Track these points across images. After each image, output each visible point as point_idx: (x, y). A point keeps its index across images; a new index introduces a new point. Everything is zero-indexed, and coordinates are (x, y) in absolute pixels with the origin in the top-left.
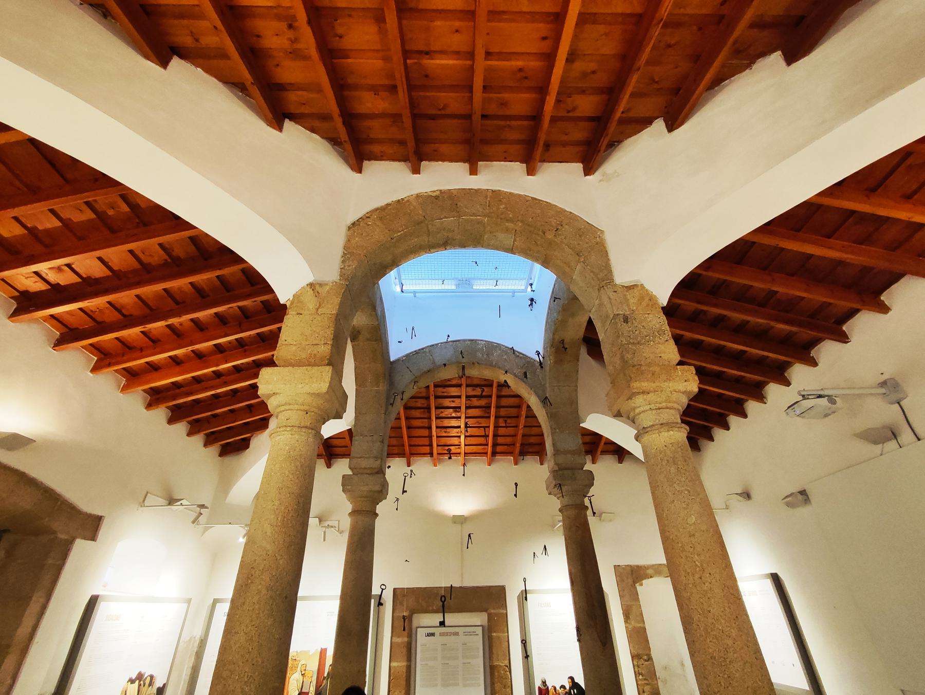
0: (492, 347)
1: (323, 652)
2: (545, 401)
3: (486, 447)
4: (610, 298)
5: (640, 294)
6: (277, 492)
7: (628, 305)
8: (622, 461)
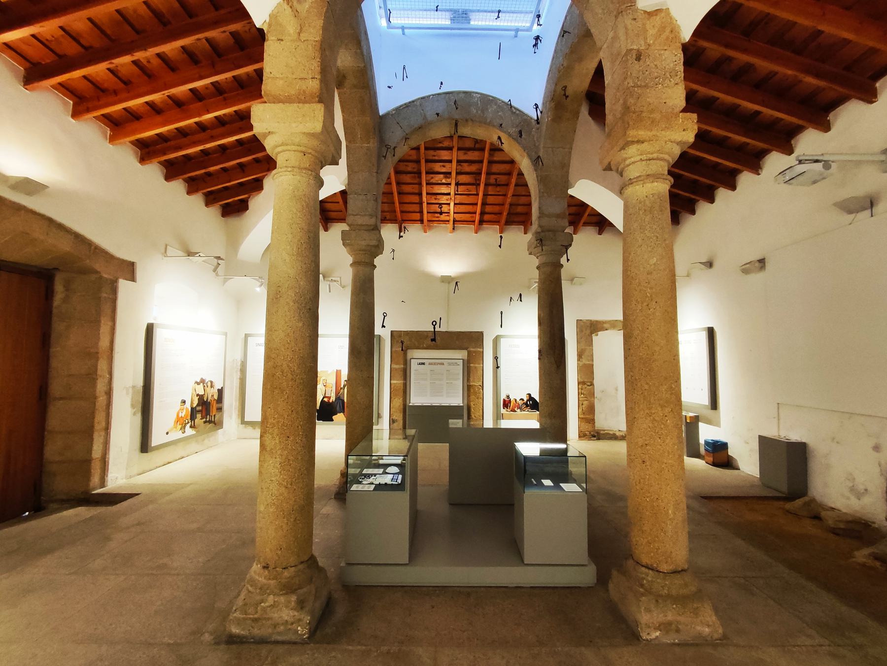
0: (487, 101)
1: (338, 374)
2: (537, 161)
3: (475, 215)
4: (626, 28)
5: (662, 23)
6: (289, 227)
7: (645, 39)
8: (602, 233)
